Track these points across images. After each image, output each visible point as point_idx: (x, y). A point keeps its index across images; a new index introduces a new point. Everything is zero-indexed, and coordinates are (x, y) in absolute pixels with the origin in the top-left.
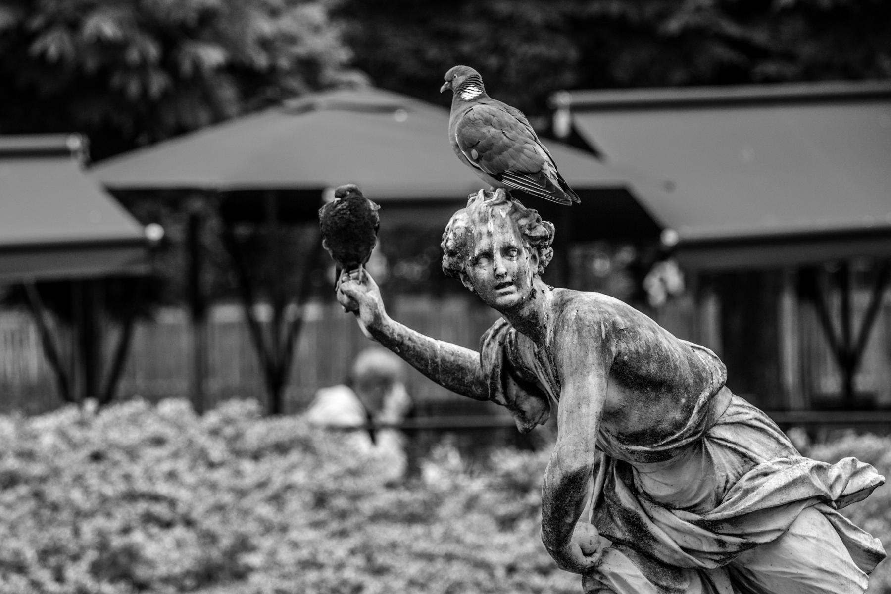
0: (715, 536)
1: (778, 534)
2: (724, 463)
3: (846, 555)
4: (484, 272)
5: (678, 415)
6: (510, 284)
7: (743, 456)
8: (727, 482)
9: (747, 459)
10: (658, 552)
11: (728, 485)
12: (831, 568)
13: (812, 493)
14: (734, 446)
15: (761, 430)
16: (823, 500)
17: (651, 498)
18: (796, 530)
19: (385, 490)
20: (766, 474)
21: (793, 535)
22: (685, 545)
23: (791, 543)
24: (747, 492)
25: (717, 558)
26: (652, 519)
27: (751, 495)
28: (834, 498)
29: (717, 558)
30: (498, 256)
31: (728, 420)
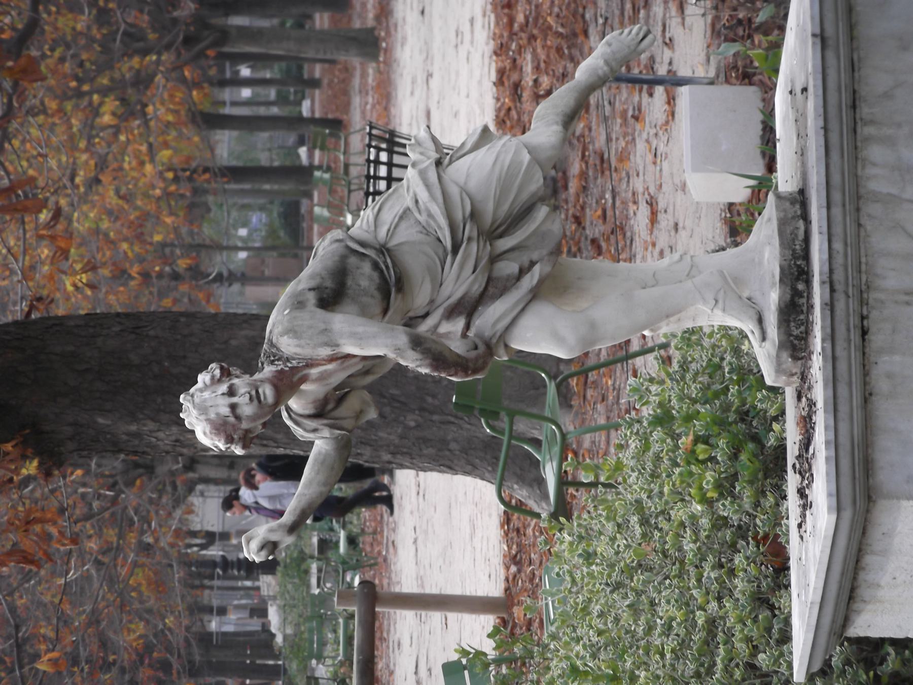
0: (464, 244)
1: (464, 194)
2: (406, 234)
3: (483, 151)
4: (247, 410)
5: (367, 267)
6: (257, 392)
7: (401, 218)
8: (421, 232)
9: (406, 214)
10: (477, 289)
11: (425, 231)
12: (494, 155)
13: (433, 168)
14: (397, 219)
15: (380, 210)
16: (438, 163)
17: (432, 301)
18: (462, 181)
19: (484, 123)
20: (417, 202)
21: (418, 475)
22: (471, 271)
23: (472, 185)
24: (430, 215)
25: (482, 243)
26: (449, 298)
27: (432, 212)
28: (438, 156)
29: (482, 243)
30: (235, 400)
31: (372, 228)
